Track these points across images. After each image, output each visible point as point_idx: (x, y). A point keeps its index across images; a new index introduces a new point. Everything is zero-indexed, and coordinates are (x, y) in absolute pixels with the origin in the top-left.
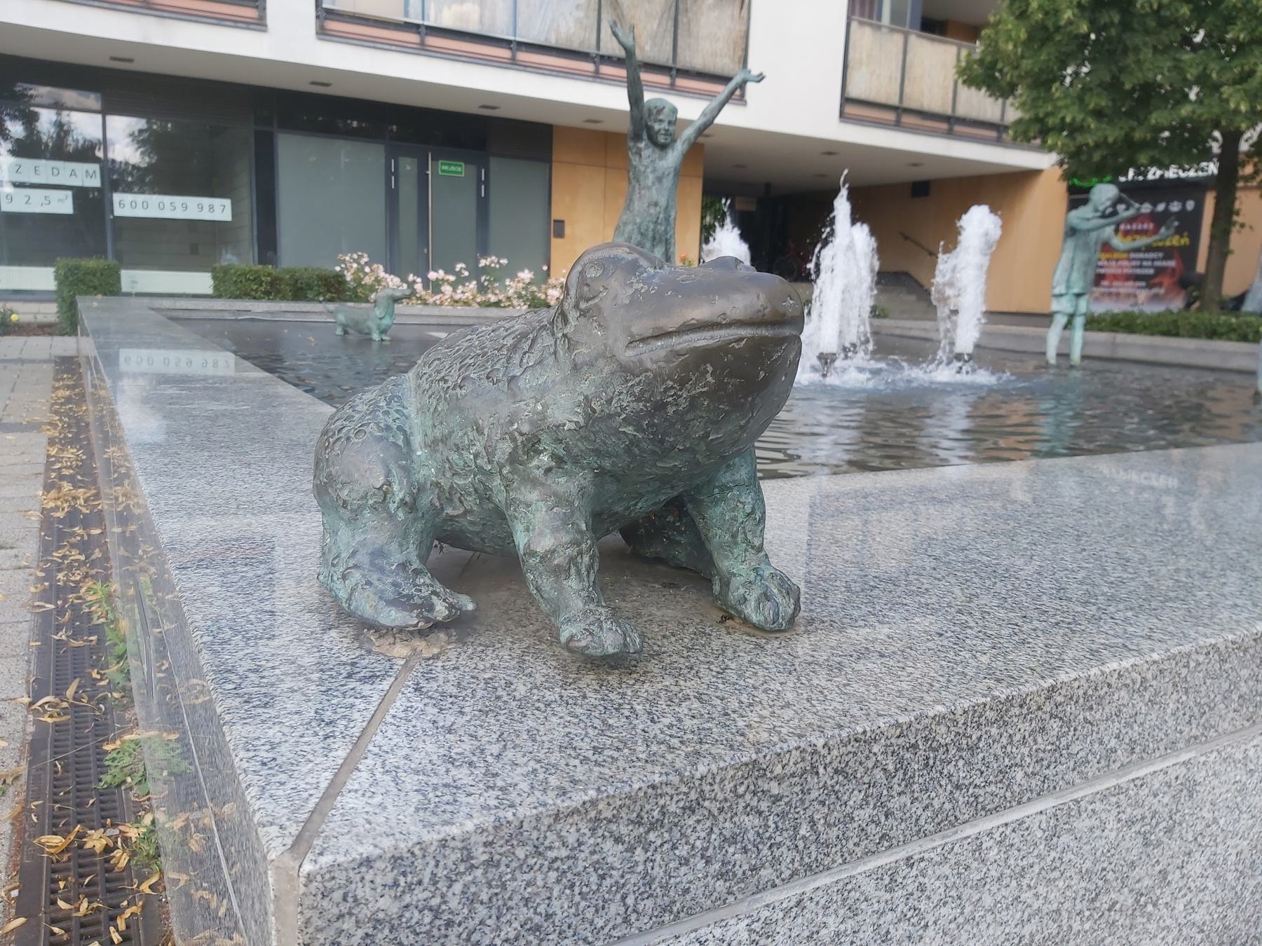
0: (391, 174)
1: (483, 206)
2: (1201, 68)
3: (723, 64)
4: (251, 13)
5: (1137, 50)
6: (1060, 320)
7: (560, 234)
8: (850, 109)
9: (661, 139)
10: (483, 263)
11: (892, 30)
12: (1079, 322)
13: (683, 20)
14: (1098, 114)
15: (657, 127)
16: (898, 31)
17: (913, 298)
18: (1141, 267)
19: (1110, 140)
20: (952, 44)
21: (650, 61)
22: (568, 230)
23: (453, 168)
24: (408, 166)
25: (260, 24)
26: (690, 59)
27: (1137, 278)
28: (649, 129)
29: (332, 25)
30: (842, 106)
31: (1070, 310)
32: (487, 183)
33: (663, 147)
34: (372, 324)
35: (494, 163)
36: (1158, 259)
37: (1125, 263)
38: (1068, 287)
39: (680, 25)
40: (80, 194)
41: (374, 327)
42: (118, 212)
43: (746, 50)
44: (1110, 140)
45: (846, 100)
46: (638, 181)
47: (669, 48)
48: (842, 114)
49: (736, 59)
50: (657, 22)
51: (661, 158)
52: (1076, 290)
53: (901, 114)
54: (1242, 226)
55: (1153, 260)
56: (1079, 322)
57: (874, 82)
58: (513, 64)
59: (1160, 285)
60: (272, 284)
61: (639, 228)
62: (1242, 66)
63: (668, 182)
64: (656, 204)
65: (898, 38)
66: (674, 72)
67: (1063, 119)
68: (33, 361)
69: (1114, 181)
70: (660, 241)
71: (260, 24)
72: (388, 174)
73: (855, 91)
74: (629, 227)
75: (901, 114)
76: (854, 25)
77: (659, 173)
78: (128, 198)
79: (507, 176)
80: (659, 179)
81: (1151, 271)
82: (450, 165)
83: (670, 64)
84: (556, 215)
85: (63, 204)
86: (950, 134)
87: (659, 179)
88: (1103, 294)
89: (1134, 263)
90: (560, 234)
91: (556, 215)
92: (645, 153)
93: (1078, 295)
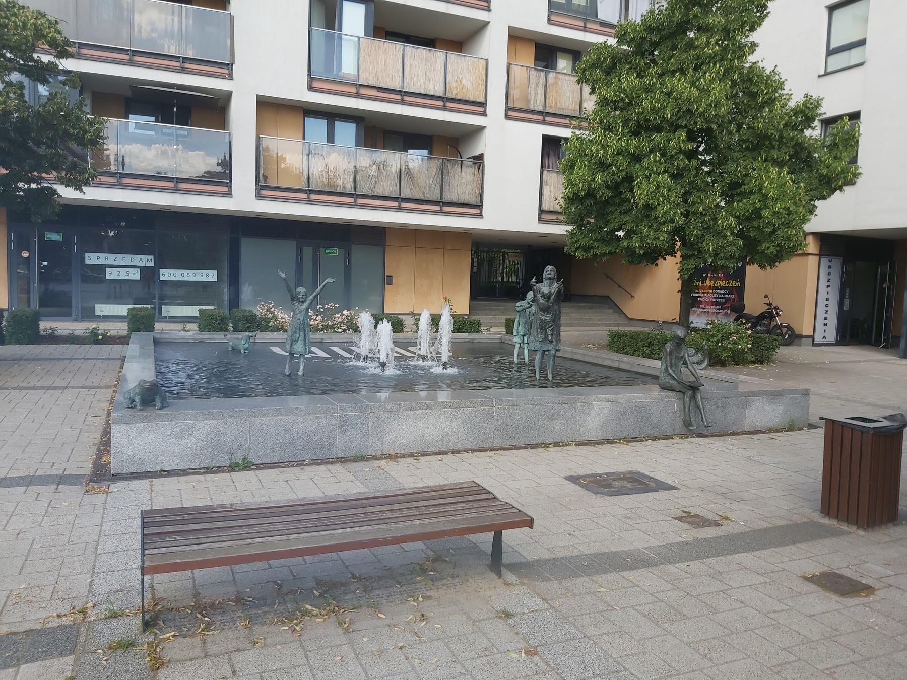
0: (299, 256)
1: (348, 269)
4: (225, 189)
7: (390, 283)
13: (446, 178)
17: (611, 311)
18: (718, 298)
22: (394, 281)
24: (308, 251)
25: (229, 194)
27: (717, 304)
29: (264, 193)
30: (539, 215)
32: (302, 255)
33: (303, 302)
34: (241, 347)
35: (355, 248)
37: (711, 295)
40: (143, 270)
42: (162, 278)
47: (439, 192)
55: (724, 294)
60: (221, 320)
68: (113, 359)
71: (229, 194)
72: (297, 256)
76: (545, 173)
78: (166, 271)
79: (360, 255)
85: (135, 275)
88: (701, 312)
90: (390, 283)
93: (523, 336)
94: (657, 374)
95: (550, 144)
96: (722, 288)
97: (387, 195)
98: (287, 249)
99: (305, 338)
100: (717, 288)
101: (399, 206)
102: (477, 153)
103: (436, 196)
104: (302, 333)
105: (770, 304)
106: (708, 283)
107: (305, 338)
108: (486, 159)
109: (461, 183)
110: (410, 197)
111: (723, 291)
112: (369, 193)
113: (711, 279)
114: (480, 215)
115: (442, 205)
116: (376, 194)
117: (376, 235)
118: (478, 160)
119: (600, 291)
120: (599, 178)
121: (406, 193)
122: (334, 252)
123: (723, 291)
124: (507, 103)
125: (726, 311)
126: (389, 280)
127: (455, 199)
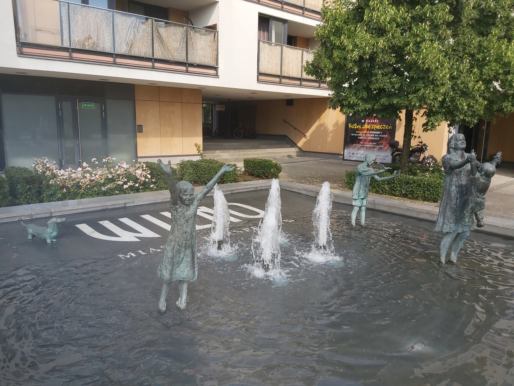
2: (400, 84)
5: (376, 75)
6: (356, 209)
7: (141, 131)
8: (261, 78)
9: (187, 202)
10: (104, 160)
11: (276, 45)
12: (363, 208)
14: (362, 99)
15: (184, 197)
19: (367, 109)
20: (300, 49)
21: (177, 60)
22: (144, 129)
23: (89, 105)
24: (67, 106)
28: (181, 198)
29: (26, 50)
31: (360, 205)
32: (105, 111)
33: (188, 205)
36: (380, 134)
38: (359, 196)
39: (189, 45)
41: (48, 237)
43: (217, 55)
44: (367, 109)
45: (260, 74)
47: (185, 55)
48: (258, 80)
49: (214, 59)
50: (179, 43)
51: (187, 210)
52: (362, 197)
53: (281, 78)
54: (415, 137)
55: (379, 134)
56: (363, 208)
57: (271, 66)
58: (115, 64)
59: (382, 144)
62: (416, 87)
65: (279, 48)
67: (349, 102)
69: (355, 73)
70: (189, 247)
73: (262, 70)
75: (281, 78)
77: (186, 219)
80: (187, 221)
81: (378, 139)
82: (87, 104)
83: (185, 61)
84: (138, 123)
87: (187, 221)
88: (361, 147)
89: (372, 135)
90: (141, 131)
91: (138, 123)
94: (434, 218)
95: (264, 21)
96: (377, 130)
97: (142, 55)
98: (47, 103)
99: (193, 258)
100: (373, 130)
101: (153, 65)
102: (210, 24)
103: (183, 59)
104: (188, 252)
105: (421, 142)
106: (366, 126)
107: (193, 258)
108: (219, 28)
109: (201, 49)
110: (162, 58)
111: (378, 133)
112: (127, 53)
113: (369, 123)
114: (217, 76)
115: (187, 66)
116: (132, 54)
117: (126, 91)
118: (213, 28)
119: (280, 132)
120: (382, 42)
121: (158, 55)
122: (91, 106)
123: (378, 133)
124: (17, 39)
125: (380, 146)
126: (140, 129)
127: (197, 61)
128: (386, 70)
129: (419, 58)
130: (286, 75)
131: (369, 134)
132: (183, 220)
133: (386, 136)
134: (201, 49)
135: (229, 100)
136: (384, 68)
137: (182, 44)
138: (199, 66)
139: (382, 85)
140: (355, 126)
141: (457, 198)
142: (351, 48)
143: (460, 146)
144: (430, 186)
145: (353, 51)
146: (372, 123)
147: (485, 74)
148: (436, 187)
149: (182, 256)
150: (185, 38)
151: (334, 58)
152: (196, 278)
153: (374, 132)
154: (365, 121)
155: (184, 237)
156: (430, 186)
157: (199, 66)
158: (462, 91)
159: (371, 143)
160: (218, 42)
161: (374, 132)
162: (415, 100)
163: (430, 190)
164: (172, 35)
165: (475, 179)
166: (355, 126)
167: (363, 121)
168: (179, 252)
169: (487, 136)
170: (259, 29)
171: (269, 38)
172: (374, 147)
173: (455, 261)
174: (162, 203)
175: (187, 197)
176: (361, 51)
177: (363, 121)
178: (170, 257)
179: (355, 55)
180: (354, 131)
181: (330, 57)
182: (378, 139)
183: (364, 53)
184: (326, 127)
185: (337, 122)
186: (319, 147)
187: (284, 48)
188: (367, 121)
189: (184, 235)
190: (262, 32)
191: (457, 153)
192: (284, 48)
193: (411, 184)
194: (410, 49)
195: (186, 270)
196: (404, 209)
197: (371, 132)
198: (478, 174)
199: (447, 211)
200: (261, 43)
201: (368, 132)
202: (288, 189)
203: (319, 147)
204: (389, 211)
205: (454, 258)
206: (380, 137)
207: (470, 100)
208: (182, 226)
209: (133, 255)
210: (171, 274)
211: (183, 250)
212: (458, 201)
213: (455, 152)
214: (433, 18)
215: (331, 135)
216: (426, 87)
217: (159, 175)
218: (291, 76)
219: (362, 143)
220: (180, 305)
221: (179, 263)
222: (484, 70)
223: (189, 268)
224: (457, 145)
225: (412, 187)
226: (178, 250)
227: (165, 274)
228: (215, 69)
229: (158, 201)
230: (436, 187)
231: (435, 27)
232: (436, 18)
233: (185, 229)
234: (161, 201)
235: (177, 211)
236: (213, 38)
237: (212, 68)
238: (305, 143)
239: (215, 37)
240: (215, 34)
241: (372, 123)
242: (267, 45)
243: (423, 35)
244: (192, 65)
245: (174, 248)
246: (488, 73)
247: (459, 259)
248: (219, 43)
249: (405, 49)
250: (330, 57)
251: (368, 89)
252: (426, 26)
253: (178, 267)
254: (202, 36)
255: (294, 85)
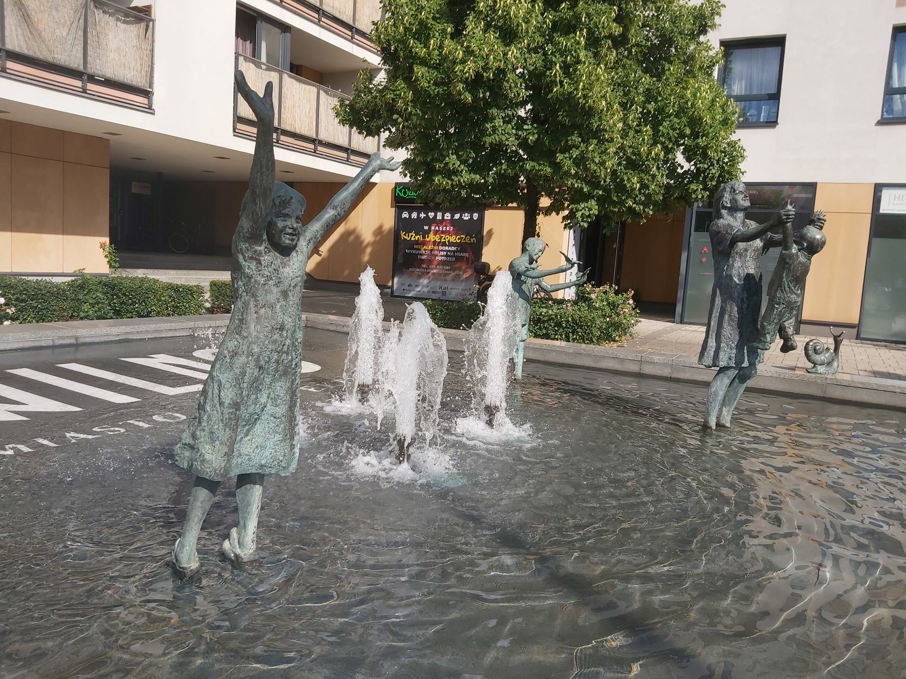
3: (139, 81)
11: (268, 69)
16: (275, 70)
26: (98, 67)
39: (89, 35)
46: (254, 296)
47: (80, 55)
48: (234, 131)
49: (143, 73)
50: (66, 29)
51: (284, 265)
55: (454, 252)
61: (257, 360)
63: (295, 298)
64: (282, 328)
66: (85, 77)
74: (242, 360)
77: (284, 287)
80: (285, 294)
86: (314, 153)
87: (285, 294)
89: (442, 253)
92: (266, 259)
100: (444, 244)
106: (432, 237)
108: (158, 14)
110: (25, 51)
111: (453, 249)
113: (436, 232)
114: (149, 109)
115: (83, 78)
123: (453, 249)
128: (510, 113)
129: (576, 89)
130: (288, 128)
131: (438, 250)
132: (275, 290)
133: (467, 255)
134: (116, 50)
135: (160, 174)
136: (506, 108)
137: (73, 30)
138: (109, 83)
139: (504, 139)
140: (413, 237)
141: (742, 299)
142: (460, 56)
143: (742, 202)
144: (577, 324)
145: (463, 62)
146: (443, 232)
147: (663, 135)
148: (588, 326)
149: (263, 399)
150: (82, 20)
151: (417, 80)
152: (294, 465)
153: (447, 248)
154: (430, 228)
155: (275, 341)
156: (577, 324)
157: (109, 83)
158: (628, 159)
159: (441, 267)
160: (153, 41)
161: (447, 248)
162: (568, 162)
163: (578, 332)
164: (51, 7)
165: (791, 256)
166: (413, 237)
167: (426, 228)
168: (256, 385)
169: (620, 259)
170: (237, 35)
171: (255, 53)
172: (446, 275)
173: (728, 425)
174: (53, 347)
175: (288, 223)
176: (481, 63)
177: (426, 228)
178: (227, 402)
179: (470, 68)
180: (412, 244)
181: (410, 81)
182: (454, 259)
183: (486, 68)
184: (358, 238)
185: (380, 227)
186: (346, 272)
187: (285, 77)
188: (433, 228)
189: (276, 336)
190: (240, 41)
191: (735, 218)
192: (285, 77)
193: (544, 322)
194: (555, 74)
195: (270, 444)
196: (569, 353)
197: (441, 248)
198: (794, 249)
199: (725, 325)
200: (241, 59)
201: (436, 248)
202: (332, 328)
203: (346, 272)
204: (542, 358)
205: (727, 421)
206: (457, 257)
207: (642, 175)
208: (272, 307)
209: (24, 449)
210: (229, 455)
211: (268, 380)
212: (745, 306)
213: (732, 215)
214: (591, 26)
215: (369, 250)
216: (586, 141)
217: (23, 301)
218: (298, 131)
219: (424, 266)
220: (238, 551)
221: (253, 421)
222: (661, 128)
223: (278, 437)
224: (736, 201)
225: (546, 328)
226: (256, 379)
227: (208, 457)
228: (147, 94)
229: (43, 344)
230: (588, 326)
231: (593, 42)
232: (597, 26)
233: (280, 317)
234: (50, 343)
235: (259, 262)
236: (142, 31)
237: (141, 93)
238: (319, 265)
239: (147, 30)
240: (147, 26)
241: (443, 232)
242: (252, 66)
243: (576, 52)
244: (92, 79)
245: (243, 374)
246: (668, 134)
247: (734, 419)
248: (156, 44)
249: (548, 73)
250: (410, 81)
251: (477, 146)
252: (581, 37)
253: (247, 435)
254: (119, 23)
255: (303, 151)
